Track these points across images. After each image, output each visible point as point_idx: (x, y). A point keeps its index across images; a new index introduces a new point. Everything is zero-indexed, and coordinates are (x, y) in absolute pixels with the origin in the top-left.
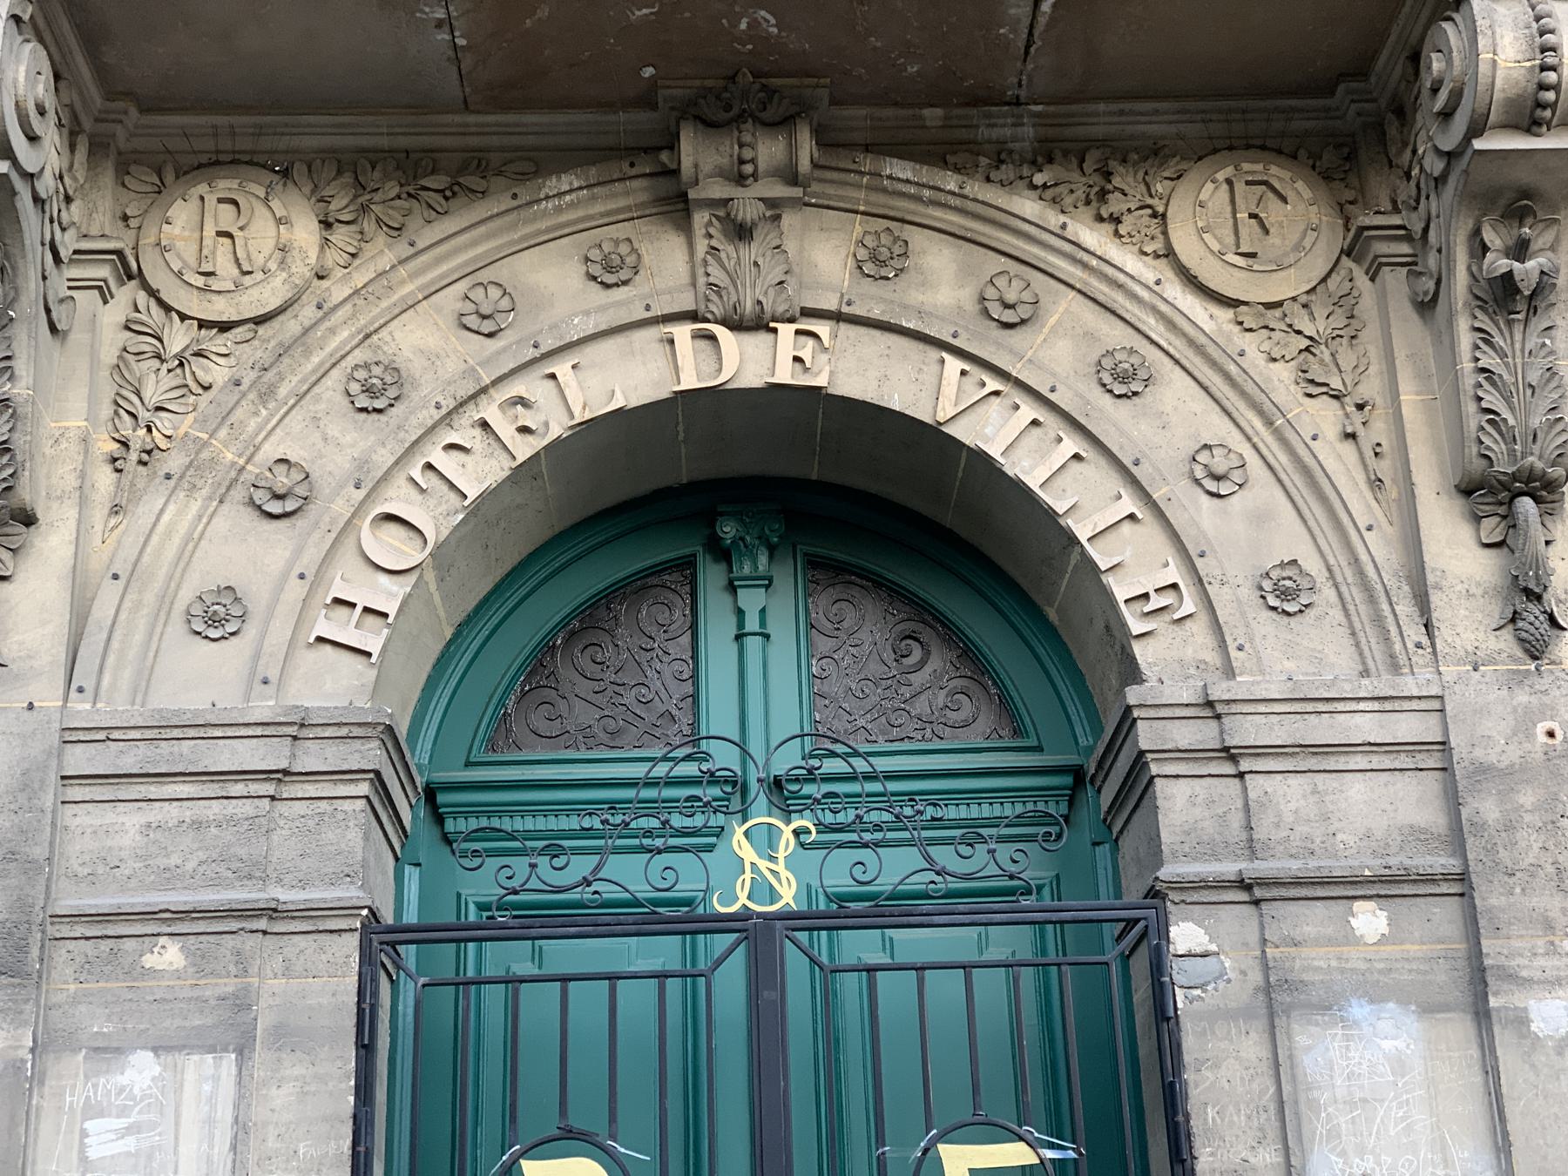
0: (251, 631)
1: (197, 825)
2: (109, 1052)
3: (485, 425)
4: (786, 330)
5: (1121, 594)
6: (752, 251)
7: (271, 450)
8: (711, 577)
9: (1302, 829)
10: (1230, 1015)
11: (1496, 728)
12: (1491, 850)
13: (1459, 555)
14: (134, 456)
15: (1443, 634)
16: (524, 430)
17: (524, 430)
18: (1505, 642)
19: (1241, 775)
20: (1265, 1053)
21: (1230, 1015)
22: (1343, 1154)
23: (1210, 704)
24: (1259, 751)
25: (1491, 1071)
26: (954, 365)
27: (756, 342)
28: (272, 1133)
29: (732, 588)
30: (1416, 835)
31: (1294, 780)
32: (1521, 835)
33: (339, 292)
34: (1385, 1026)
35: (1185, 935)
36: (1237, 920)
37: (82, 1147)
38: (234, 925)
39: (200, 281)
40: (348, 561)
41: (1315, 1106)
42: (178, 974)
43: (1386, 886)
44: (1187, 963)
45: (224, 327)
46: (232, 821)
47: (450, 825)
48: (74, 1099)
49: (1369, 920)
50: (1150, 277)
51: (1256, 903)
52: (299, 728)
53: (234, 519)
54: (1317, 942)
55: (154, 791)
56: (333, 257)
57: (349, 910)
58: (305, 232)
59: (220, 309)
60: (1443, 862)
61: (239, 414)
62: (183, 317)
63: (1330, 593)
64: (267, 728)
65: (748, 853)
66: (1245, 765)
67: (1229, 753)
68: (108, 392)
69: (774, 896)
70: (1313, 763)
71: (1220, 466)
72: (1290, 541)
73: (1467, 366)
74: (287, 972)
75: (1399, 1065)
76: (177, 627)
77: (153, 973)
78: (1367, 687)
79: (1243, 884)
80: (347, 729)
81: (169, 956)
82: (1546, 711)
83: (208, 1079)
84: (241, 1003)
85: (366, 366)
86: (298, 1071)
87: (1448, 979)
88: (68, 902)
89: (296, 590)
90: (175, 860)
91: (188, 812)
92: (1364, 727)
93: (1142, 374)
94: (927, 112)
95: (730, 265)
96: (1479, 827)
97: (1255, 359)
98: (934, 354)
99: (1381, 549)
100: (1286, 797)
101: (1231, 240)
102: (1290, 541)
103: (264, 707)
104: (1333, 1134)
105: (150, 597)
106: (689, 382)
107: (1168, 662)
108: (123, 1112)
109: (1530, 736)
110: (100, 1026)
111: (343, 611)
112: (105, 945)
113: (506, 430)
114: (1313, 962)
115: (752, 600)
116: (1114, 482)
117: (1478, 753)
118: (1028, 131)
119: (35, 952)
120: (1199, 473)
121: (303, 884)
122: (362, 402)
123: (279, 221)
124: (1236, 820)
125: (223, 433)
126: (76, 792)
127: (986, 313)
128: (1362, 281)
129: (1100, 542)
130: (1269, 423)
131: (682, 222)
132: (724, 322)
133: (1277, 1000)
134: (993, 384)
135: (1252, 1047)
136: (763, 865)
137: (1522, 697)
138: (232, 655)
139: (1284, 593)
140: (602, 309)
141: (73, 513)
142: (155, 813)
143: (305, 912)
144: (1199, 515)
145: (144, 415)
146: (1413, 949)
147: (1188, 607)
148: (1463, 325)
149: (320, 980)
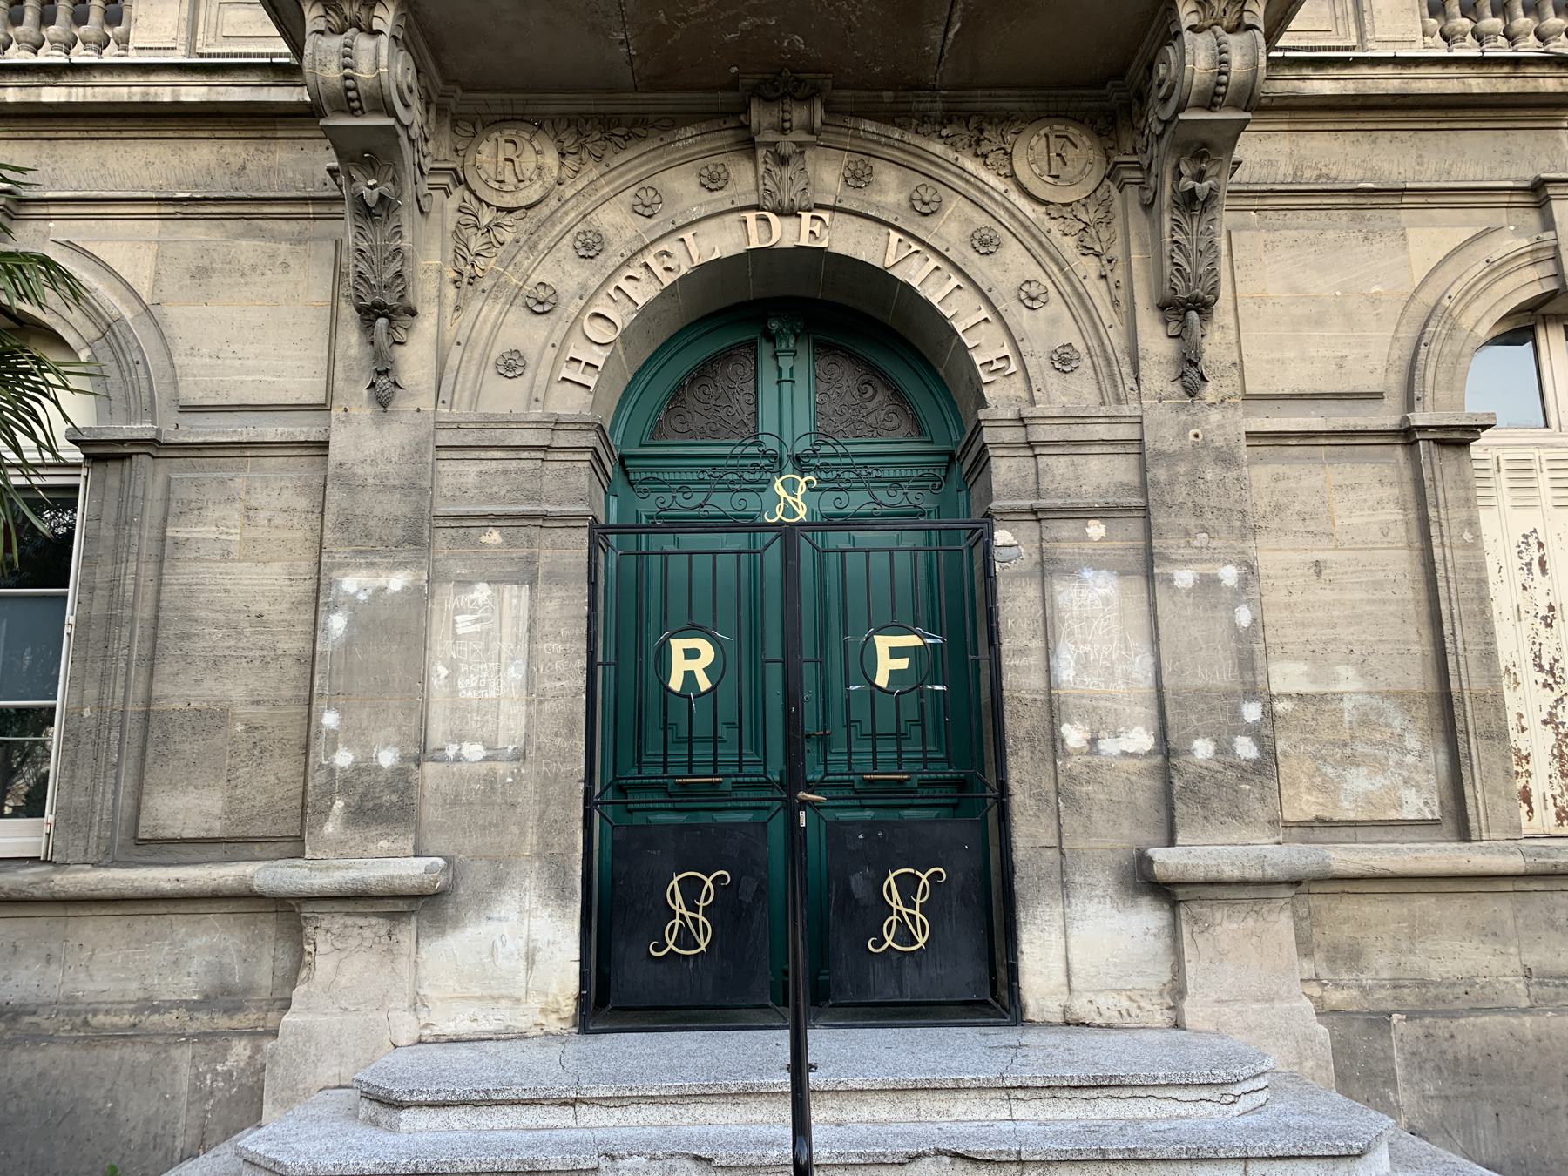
0: (528, 374)
1: (505, 472)
2: (466, 583)
3: (646, 266)
4: (806, 216)
5: (978, 361)
6: (788, 172)
7: (536, 278)
8: (765, 350)
9: (1065, 484)
10: (1022, 575)
11: (1168, 432)
12: (1161, 495)
13: (1156, 342)
14: (465, 280)
15: (1145, 384)
16: (668, 269)
17: (668, 269)
18: (1177, 388)
19: (1035, 456)
20: (1038, 594)
21: (1022, 575)
22: (1075, 643)
23: (1021, 419)
24: (1045, 444)
25: (1152, 604)
26: (895, 236)
27: (790, 222)
28: (547, 623)
29: (776, 357)
30: (1123, 487)
31: (1062, 459)
32: (1177, 487)
33: (569, 193)
34: (1100, 582)
35: (1002, 536)
36: (1029, 529)
37: (454, 628)
38: (526, 523)
39: (497, 186)
40: (577, 337)
41: (1062, 620)
42: (498, 546)
43: (1105, 512)
44: (1002, 550)
45: (510, 211)
46: (522, 471)
47: (632, 476)
48: (449, 606)
49: (1096, 529)
50: (1002, 188)
51: (1039, 520)
52: (555, 424)
53: (517, 314)
54: (1068, 540)
55: (483, 455)
56: (566, 173)
57: (583, 517)
58: (551, 160)
59: (508, 201)
60: (1136, 501)
61: (519, 258)
62: (489, 205)
63: (1087, 361)
64: (539, 424)
65: (782, 493)
66: (1037, 451)
67: (1030, 445)
68: (451, 245)
69: (795, 515)
70: (1073, 450)
71: (1034, 292)
72: (1068, 333)
73: (1168, 239)
74: (553, 546)
75: (1107, 601)
76: (491, 371)
77: (486, 545)
78: (1104, 411)
79: (1033, 511)
80: (579, 426)
81: (494, 537)
82: (1195, 424)
83: (515, 597)
84: (530, 561)
85: (584, 233)
86: (560, 594)
87: (1134, 560)
88: (441, 510)
89: (551, 353)
90: (495, 489)
91: (501, 466)
92: (1101, 431)
93: (995, 242)
94: (885, 94)
95: (777, 179)
96: (1156, 483)
97: (1056, 234)
98: (884, 230)
99: (1116, 338)
100: (1058, 467)
101: (1046, 168)
102: (1068, 333)
103: (536, 413)
104: (1071, 633)
105: (477, 355)
106: (754, 244)
107: (1001, 396)
108: (473, 612)
109: (1186, 437)
110: (461, 570)
111: (575, 364)
112: (462, 531)
113: (658, 270)
114: (1066, 550)
115: (786, 363)
116: (977, 301)
117: (1158, 445)
118: (939, 105)
119: (427, 533)
120: (1023, 296)
121: (560, 503)
122: (583, 252)
123: (537, 153)
124: (1031, 479)
125: (511, 268)
126: (443, 455)
127: (913, 207)
128: (1114, 191)
129: (969, 333)
130: (1061, 269)
131: (753, 157)
132: (773, 211)
133: (1046, 568)
134: (915, 247)
135: (1033, 591)
136: (790, 499)
137: (1183, 417)
138: (520, 385)
139: (1064, 361)
140: (708, 203)
141: (436, 310)
142: (483, 466)
143: (562, 517)
144: (1021, 319)
145: (470, 258)
146: (1117, 544)
147: (1013, 368)
148: (1167, 217)
149: (572, 549)
